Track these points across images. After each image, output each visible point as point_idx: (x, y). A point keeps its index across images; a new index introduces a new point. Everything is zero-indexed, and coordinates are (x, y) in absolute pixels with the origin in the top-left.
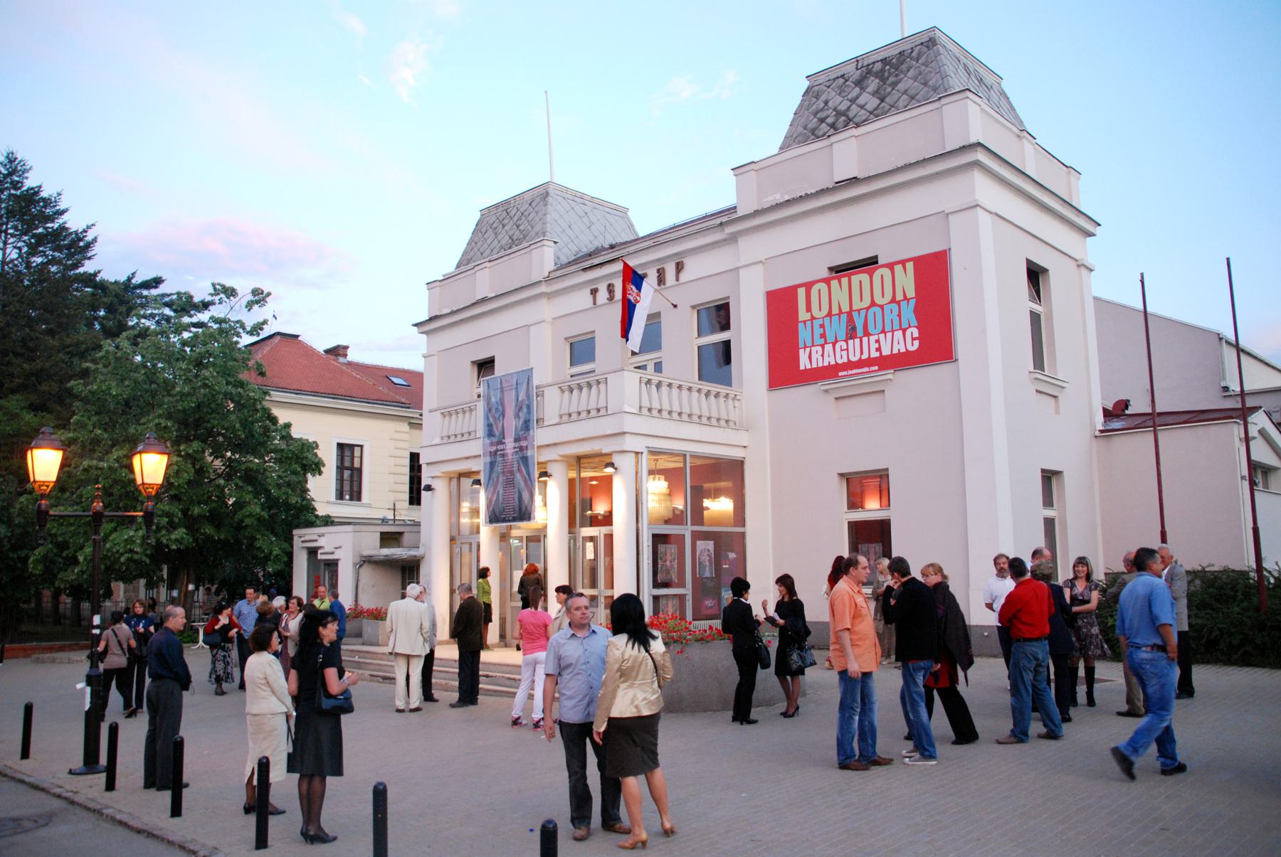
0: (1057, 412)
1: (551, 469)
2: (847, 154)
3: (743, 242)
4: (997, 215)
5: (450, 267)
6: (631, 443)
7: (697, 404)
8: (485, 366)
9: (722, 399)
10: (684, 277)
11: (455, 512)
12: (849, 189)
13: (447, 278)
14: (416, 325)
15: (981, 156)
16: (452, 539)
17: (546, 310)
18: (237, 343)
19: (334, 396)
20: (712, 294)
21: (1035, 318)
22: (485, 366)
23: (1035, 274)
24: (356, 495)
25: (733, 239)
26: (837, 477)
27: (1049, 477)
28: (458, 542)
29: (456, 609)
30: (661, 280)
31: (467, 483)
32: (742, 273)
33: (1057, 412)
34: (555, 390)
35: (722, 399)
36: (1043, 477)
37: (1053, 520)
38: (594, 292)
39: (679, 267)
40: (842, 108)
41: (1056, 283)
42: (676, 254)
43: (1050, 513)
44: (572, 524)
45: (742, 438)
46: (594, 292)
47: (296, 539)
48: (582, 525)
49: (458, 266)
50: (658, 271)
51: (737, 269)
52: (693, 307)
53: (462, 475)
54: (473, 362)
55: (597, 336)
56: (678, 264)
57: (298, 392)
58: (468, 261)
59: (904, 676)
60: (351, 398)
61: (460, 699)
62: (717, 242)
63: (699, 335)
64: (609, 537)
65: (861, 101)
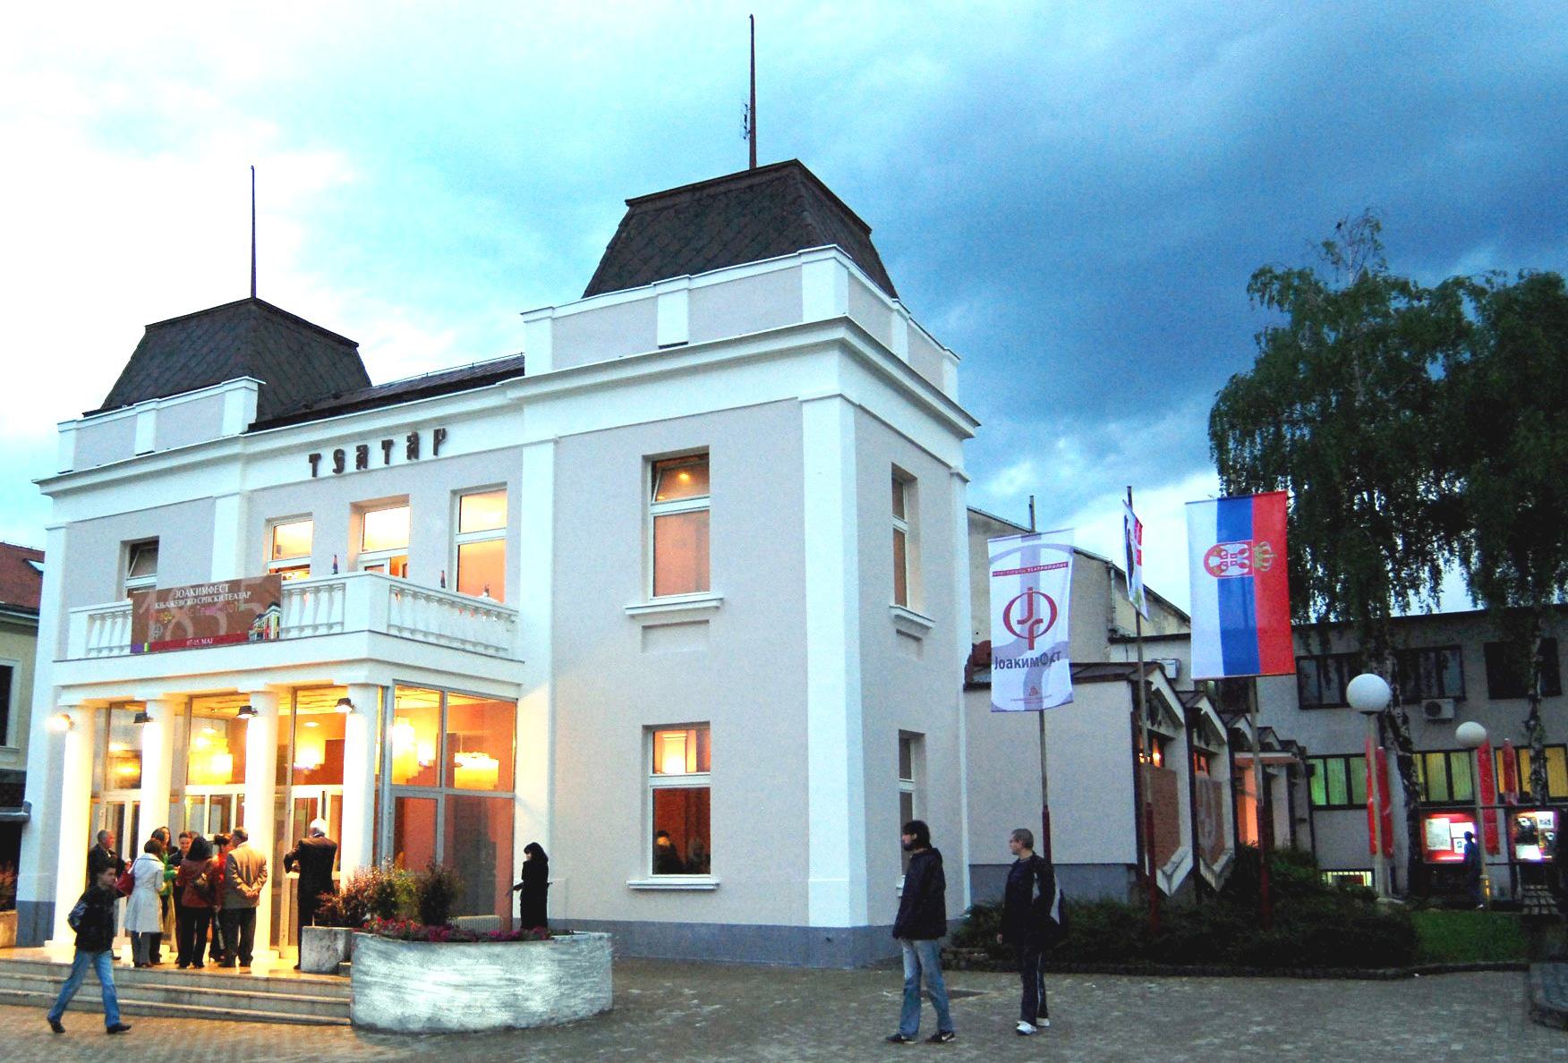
1: (151, 710)
4: (860, 407)
5: (98, 407)
8: (142, 552)
10: (446, 450)
11: (102, 755)
12: (675, 362)
14: (41, 483)
15: (841, 333)
17: (229, 481)
18: (1435, 359)
21: (899, 536)
22: (142, 552)
23: (902, 481)
25: (516, 407)
27: (909, 741)
30: (413, 451)
32: (527, 452)
36: (901, 740)
37: (910, 795)
38: (315, 459)
39: (440, 437)
42: (435, 419)
43: (907, 786)
46: (315, 459)
50: (358, 448)
53: (115, 705)
54: (124, 543)
56: (437, 432)
58: (124, 394)
59: (1026, 989)
64: (339, 799)
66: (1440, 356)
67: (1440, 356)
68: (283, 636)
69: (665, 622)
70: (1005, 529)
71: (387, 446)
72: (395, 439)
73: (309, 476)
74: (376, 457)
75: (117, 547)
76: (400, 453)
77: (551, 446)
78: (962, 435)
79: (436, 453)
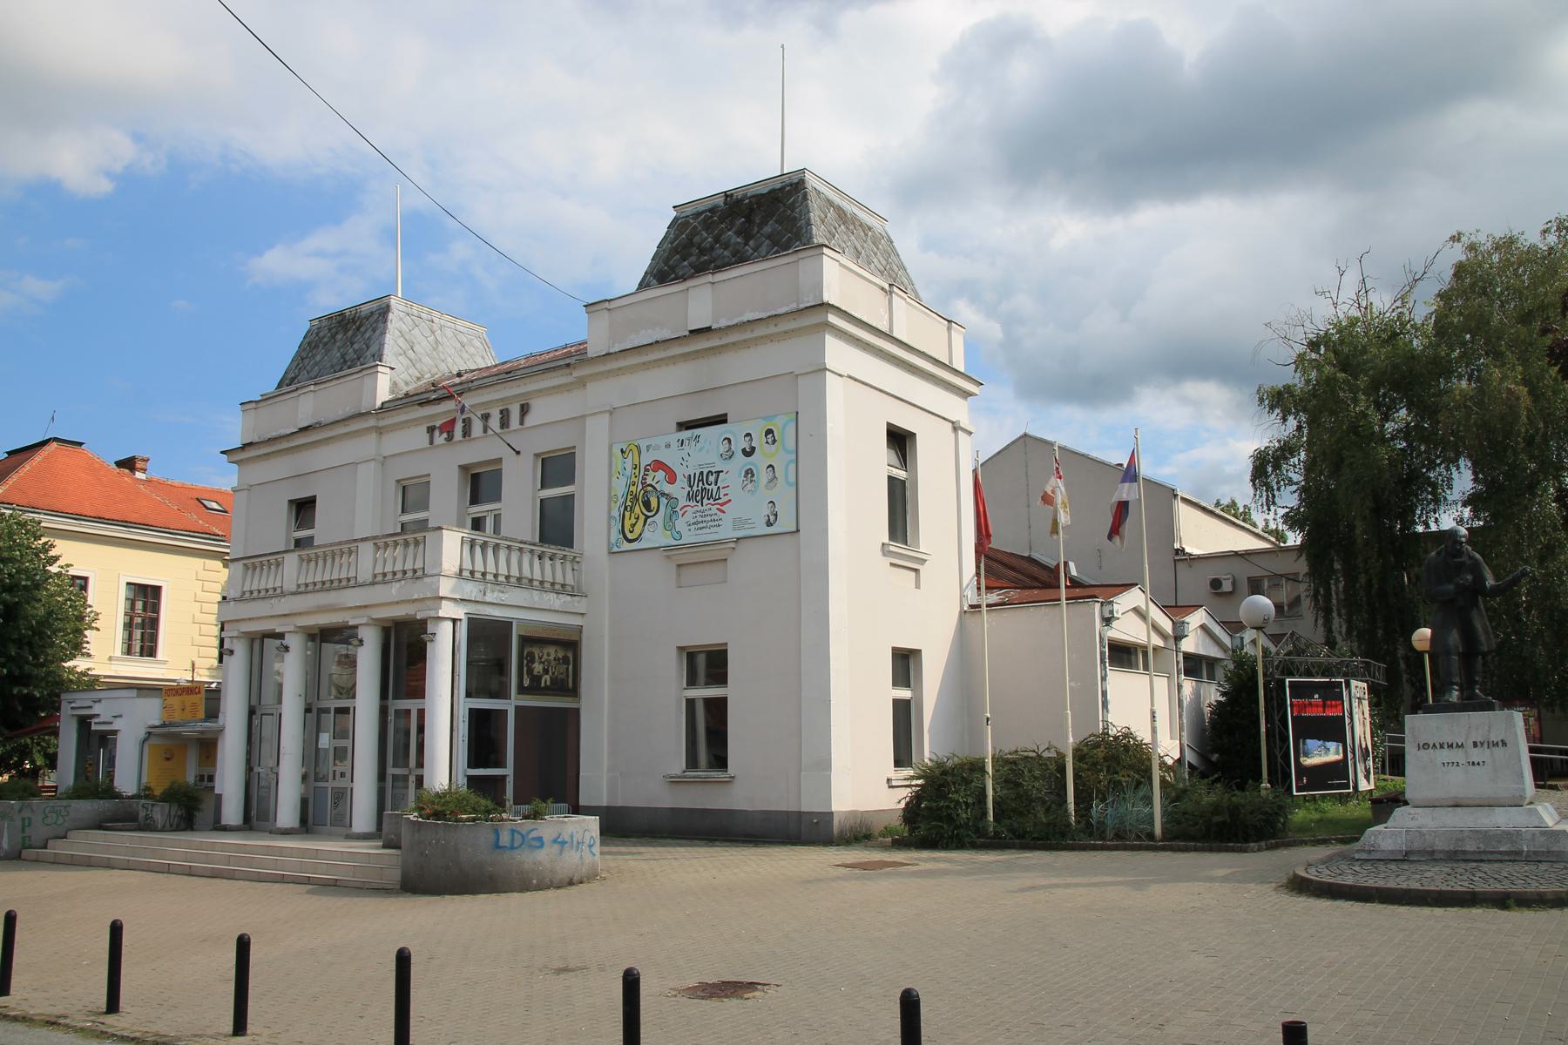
0: (918, 586)
2: (702, 301)
3: (591, 387)
5: (270, 387)
6: (448, 610)
7: (533, 569)
8: (304, 509)
9: (558, 562)
10: (530, 420)
13: (266, 398)
16: (252, 712)
19: (126, 523)
20: (552, 442)
23: (900, 440)
24: (149, 650)
25: (582, 383)
26: (674, 651)
28: (259, 713)
29: (1014, 594)
30: (505, 423)
31: (271, 644)
32: (589, 421)
33: (918, 586)
34: (369, 546)
35: (558, 562)
39: (525, 410)
40: (706, 245)
41: (924, 450)
43: (905, 694)
44: (384, 694)
45: (579, 605)
47: (64, 705)
48: (395, 698)
49: (280, 385)
51: (583, 417)
52: (537, 455)
55: (432, 480)
56: (522, 406)
57: (79, 517)
58: (291, 381)
60: (146, 526)
61: (912, 813)
62: (560, 386)
63: (543, 486)
65: (724, 238)
66: (1292, 423)
67: (1292, 423)
68: (25, 853)
69: (1459, 885)
70: (1357, 434)
71: (486, 417)
72: (510, 407)
73: (426, 444)
74: (477, 427)
75: (286, 505)
76: (494, 423)
77: (606, 418)
78: (966, 394)
79: (522, 423)
